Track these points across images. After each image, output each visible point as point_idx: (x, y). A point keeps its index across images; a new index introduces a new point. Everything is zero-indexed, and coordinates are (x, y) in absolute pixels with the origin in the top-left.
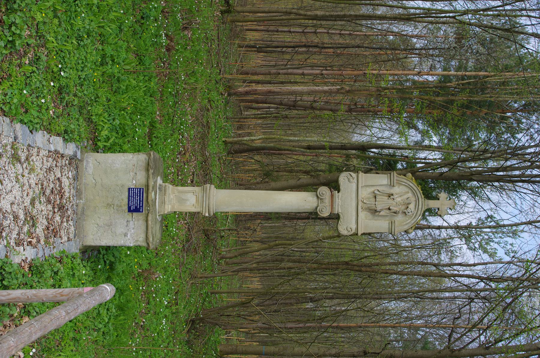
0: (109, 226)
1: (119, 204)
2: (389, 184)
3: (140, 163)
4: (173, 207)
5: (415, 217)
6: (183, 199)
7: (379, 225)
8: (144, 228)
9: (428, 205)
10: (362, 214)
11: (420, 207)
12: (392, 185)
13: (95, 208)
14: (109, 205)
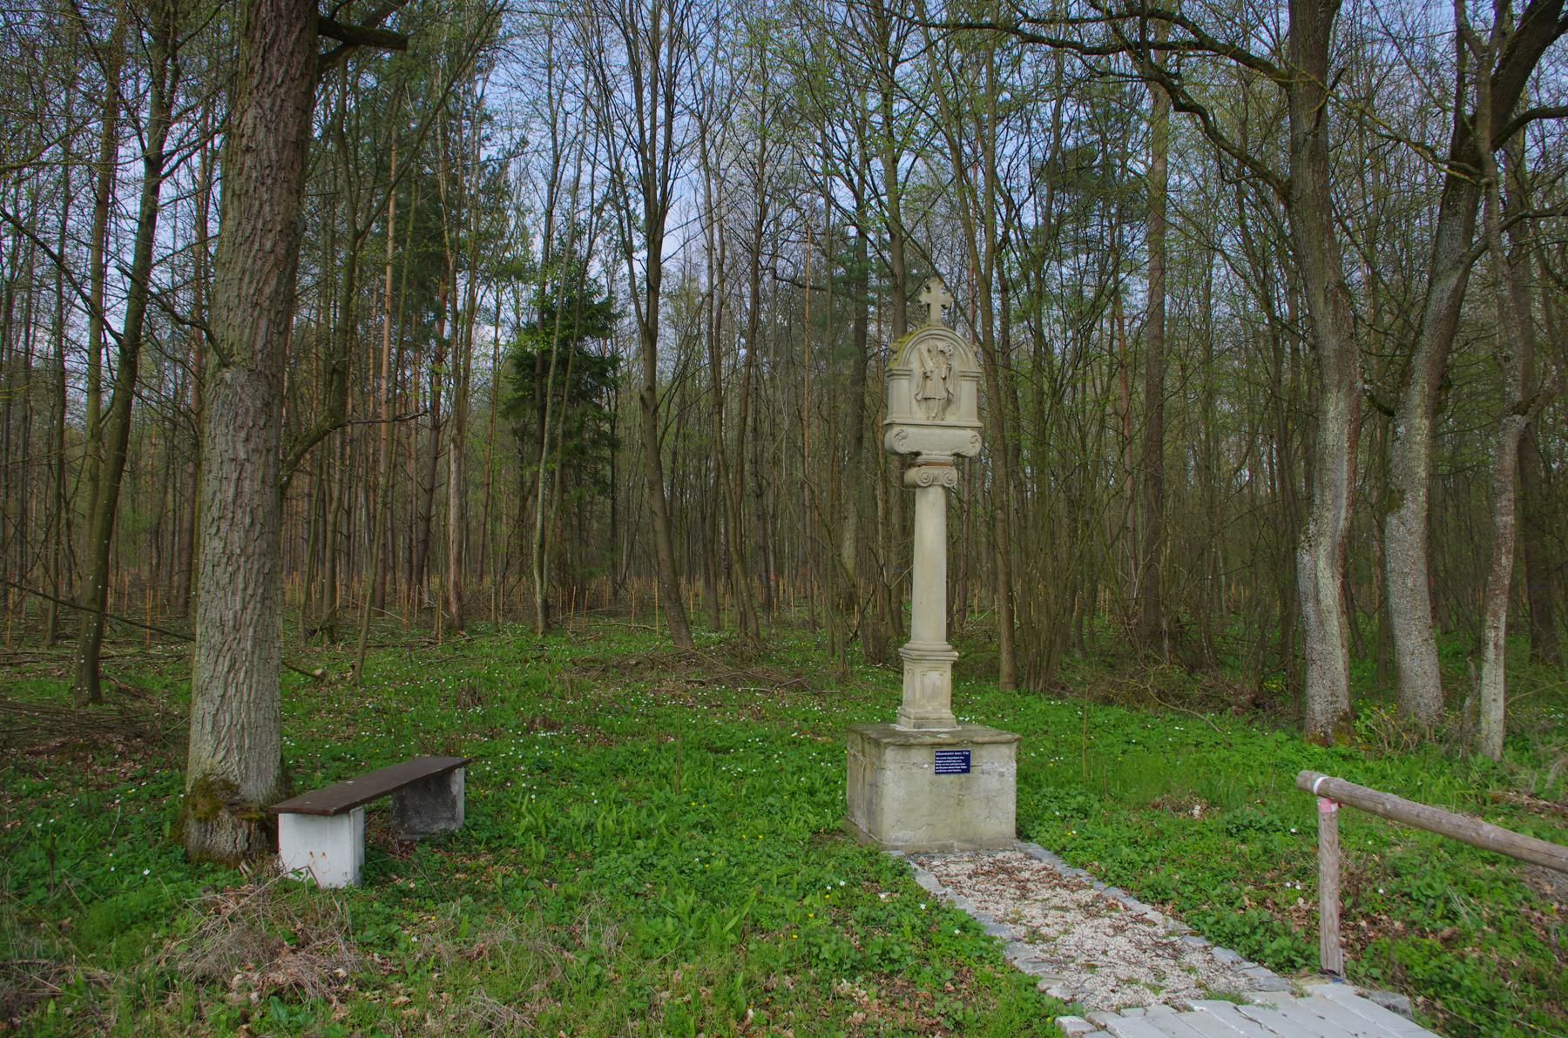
4: (944, 706)
6: (927, 689)
7: (967, 393)
8: (991, 748)
12: (909, 374)
14: (960, 803)
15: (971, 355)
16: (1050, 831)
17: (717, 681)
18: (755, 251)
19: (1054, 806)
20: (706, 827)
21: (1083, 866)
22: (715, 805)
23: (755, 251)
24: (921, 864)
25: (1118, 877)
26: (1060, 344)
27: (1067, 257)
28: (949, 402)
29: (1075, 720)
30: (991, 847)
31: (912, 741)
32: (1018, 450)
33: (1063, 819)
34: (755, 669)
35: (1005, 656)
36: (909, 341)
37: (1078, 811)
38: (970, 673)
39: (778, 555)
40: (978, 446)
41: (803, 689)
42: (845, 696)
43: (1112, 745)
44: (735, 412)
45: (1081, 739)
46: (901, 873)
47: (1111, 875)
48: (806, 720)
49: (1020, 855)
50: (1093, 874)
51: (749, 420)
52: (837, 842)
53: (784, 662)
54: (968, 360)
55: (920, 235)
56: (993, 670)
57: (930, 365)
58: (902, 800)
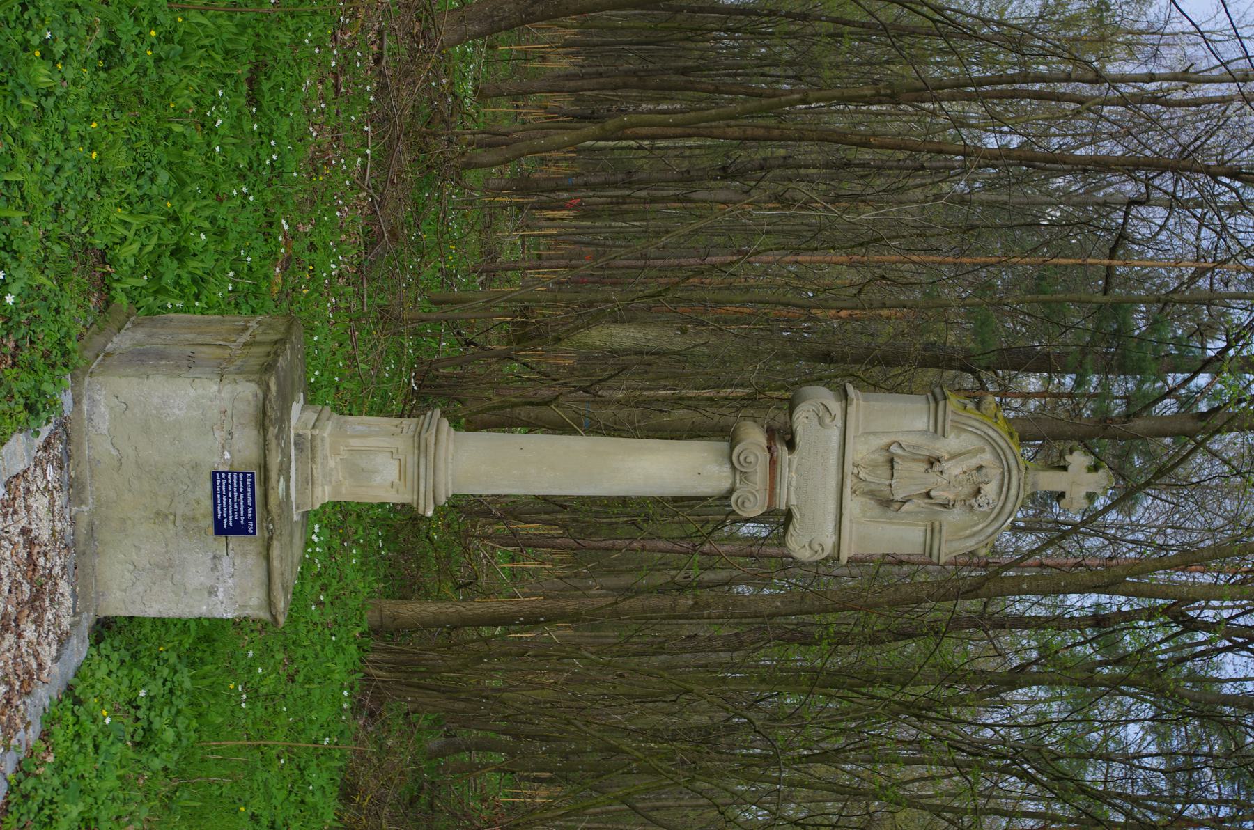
0: (164, 568)
1: (189, 514)
2: (932, 429)
3: (241, 406)
5: (996, 518)
6: (367, 461)
7: (902, 536)
8: (260, 573)
9: (1034, 484)
10: (853, 505)
11: (1013, 492)
12: (938, 431)
13: (123, 521)
14: (161, 517)
15: (970, 544)
16: (109, 679)
17: (382, 89)
18: (1182, 165)
19: (156, 688)
20: (110, 55)
21: (45, 735)
22: (152, 72)
23: (1182, 165)
24: (47, 446)
25: (26, 797)
26: (992, 722)
27: (1162, 737)
28: (886, 503)
29: (314, 732)
30: (80, 572)
31: (273, 431)
32: (806, 641)
33: (133, 704)
34: (405, 158)
35: (431, 609)
36: (998, 434)
37: (148, 730)
38: (396, 538)
39: (618, 209)
40: (804, 554)
41: (370, 245)
42: (356, 321)
43: (268, 797)
44: (877, 127)
45: (280, 740)
46: (30, 408)
47: (29, 784)
48: (312, 247)
49: (65, 624)
50: (31, 753)
51: (866, 155)
52: (87, 294)
53: (419, 213)
54: (961, 536)
55: (1200, 466)
56: (404, 586)
57: (954, 469)
58: (165, 412)
